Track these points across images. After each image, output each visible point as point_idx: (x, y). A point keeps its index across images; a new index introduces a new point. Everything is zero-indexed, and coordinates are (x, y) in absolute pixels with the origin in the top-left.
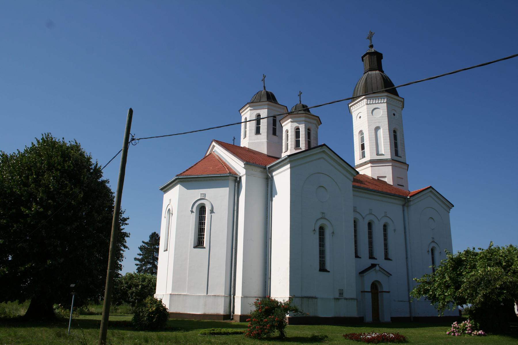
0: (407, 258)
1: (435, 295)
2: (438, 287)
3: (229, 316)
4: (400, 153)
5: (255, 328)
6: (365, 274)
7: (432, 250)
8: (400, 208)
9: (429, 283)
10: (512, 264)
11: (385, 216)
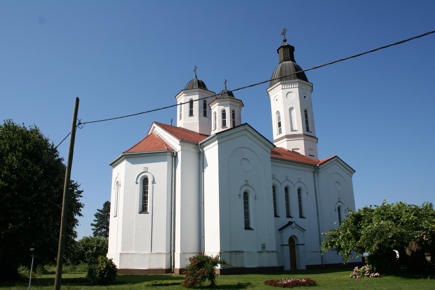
0: (318, 216)
1: (340, 246)
2: (342, 239)
3: (170, 270)
4: (310, 129)
5: (189, 279)
6: (283, 230)
7: (339, 209)
8: (312, 174)
9: (335, 236)
10: (401, 217)
11: (299, 182)
